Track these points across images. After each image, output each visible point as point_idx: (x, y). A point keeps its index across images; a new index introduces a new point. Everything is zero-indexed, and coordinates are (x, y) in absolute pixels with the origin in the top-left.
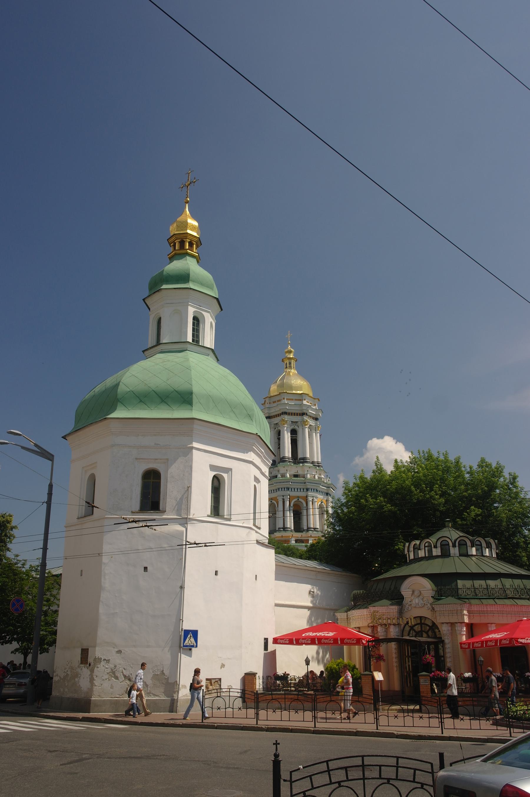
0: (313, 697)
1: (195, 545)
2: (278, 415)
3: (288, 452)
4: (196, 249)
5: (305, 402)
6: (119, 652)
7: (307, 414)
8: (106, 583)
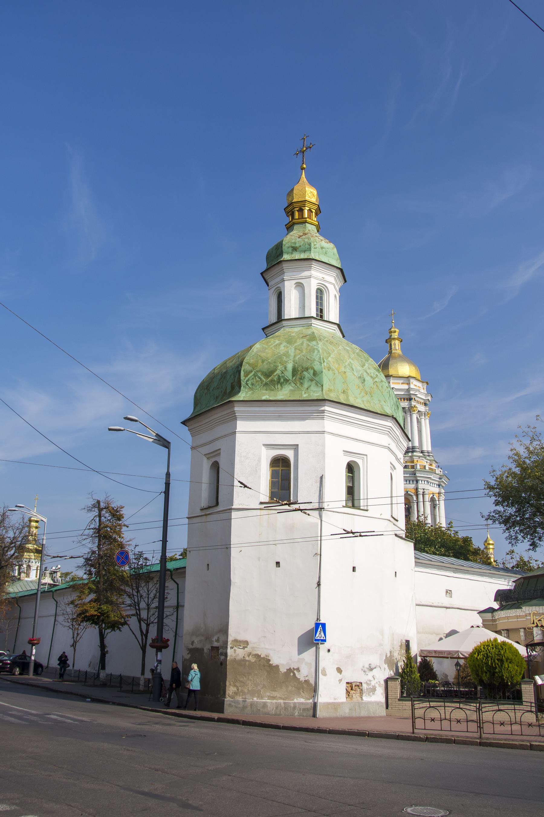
1: (351, 535)
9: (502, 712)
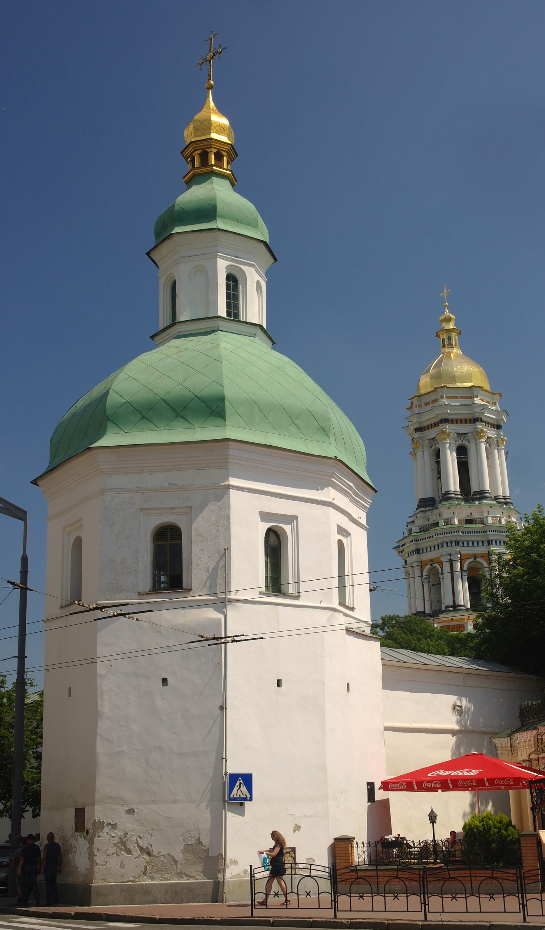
0: (421, 873)
2: (435, 425)
3: (453, 484)
4: (228, 163)
5: (477, 401)
6: (131, 811)
7: (482, 421)
8: (105, 706)
9: (494, 881)
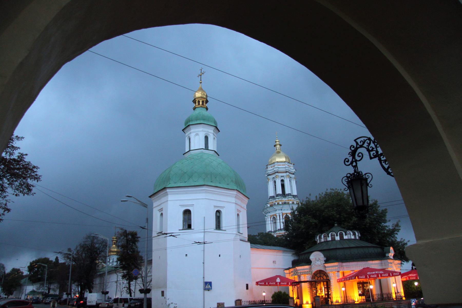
3: (279, 191)
